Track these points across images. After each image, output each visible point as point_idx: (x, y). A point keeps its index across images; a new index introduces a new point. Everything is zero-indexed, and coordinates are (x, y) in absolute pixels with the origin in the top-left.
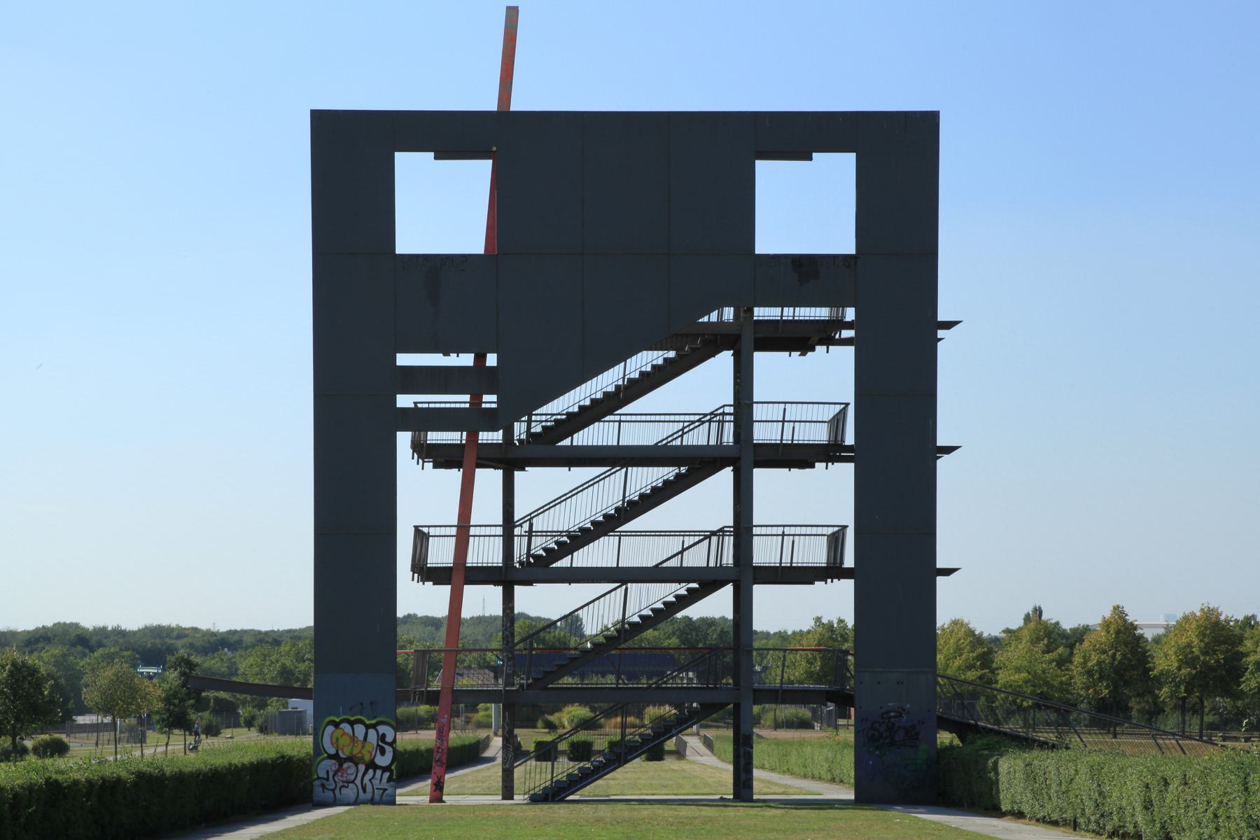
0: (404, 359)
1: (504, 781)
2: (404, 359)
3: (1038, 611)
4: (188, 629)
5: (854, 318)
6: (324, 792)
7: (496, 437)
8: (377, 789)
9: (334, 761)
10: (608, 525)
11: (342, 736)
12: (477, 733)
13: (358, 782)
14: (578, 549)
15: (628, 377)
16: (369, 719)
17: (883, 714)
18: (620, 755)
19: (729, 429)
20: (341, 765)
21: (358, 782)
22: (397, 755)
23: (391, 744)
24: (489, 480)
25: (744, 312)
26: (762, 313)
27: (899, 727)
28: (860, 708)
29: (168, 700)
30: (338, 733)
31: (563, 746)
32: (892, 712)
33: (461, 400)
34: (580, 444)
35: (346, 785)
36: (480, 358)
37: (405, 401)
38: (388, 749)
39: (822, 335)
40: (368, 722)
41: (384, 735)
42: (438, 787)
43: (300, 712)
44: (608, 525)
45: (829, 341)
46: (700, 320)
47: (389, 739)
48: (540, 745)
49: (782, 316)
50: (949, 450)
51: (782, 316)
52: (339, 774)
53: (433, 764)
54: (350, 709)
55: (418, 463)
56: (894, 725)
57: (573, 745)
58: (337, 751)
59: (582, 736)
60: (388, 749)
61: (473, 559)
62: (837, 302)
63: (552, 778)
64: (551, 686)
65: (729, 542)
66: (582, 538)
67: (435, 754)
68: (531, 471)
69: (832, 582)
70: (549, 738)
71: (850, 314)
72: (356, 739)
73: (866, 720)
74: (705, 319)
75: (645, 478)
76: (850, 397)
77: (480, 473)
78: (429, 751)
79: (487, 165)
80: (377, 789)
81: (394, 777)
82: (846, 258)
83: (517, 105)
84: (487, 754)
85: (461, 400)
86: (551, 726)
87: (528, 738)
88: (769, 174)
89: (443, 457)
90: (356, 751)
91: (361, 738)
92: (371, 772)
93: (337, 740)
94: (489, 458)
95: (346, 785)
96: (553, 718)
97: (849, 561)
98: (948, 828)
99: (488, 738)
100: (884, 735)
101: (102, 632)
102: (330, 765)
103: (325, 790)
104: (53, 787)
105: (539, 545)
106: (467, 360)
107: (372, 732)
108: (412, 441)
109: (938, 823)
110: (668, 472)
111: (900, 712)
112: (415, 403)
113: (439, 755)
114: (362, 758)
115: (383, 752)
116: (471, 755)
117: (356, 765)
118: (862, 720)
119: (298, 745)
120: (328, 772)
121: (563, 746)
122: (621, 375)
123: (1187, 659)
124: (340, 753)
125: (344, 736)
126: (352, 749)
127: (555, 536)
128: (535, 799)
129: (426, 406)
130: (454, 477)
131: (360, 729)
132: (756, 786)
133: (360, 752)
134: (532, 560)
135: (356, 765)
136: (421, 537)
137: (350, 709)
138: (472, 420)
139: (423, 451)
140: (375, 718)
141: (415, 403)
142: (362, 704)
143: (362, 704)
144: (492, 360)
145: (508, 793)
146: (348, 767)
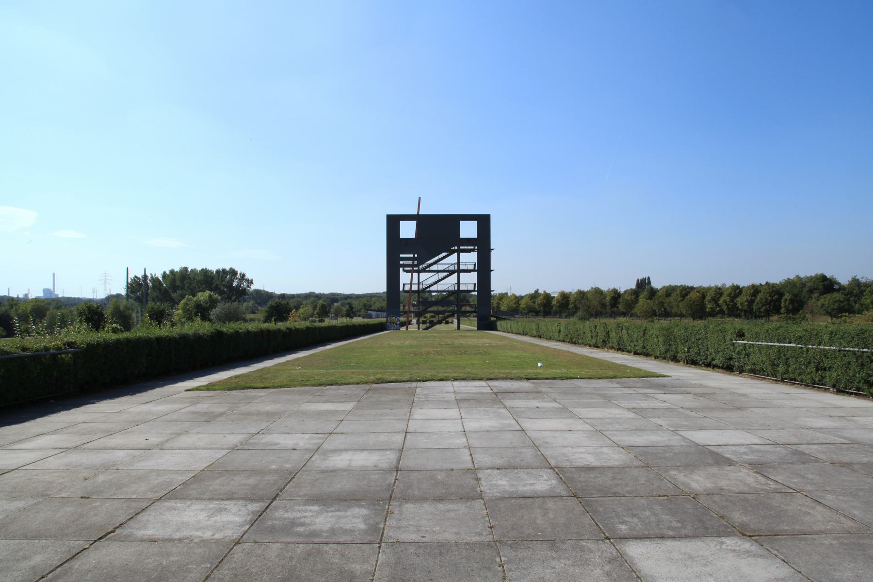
0: (401, 256)
2: (401, 256)
3: (538, 290)
10: (436, 283)
18: (440, 322)
19: (456, 266)
24: (415, 275)
25: (459, 247)
26: (461, 247)
29: (347, 311)
31: (428, 321)
33: (411, 262)
36: (414, 255)
37: (401, 262)
39: (473, 250)
42: (407, 327)
44: (436, 283)
45: (474, 251)
48: (423, 321)
50: (493, 270)
57: (430, 321)
59: (432, 319)
61: (413, 289)
62: (474, 246)
65: (456, 285)
66: (431, 285)
68: (422, 273)
70: (424, 320)
71: (476, 248)
79: (415, 222)
82: (475, 238)
83: (420, 213)
84: (412, 323)
85: (411, 262)
86: (425, 317)
87: (422, 319)
88: (462, 223)
89: (407, 271)
96: (425, 315)
98: (493, 334)
102: (390, 323)
106: (412, 256)
110: (446, 274)
119: (384, 320)
121: (428, 321)
123: (558, 302)
128: (423, 330)
131: (394, 318)
136: (404, 285)
138: (413, 266)
139: (404, 271)
144: (416, 256)
145: (419, 328)
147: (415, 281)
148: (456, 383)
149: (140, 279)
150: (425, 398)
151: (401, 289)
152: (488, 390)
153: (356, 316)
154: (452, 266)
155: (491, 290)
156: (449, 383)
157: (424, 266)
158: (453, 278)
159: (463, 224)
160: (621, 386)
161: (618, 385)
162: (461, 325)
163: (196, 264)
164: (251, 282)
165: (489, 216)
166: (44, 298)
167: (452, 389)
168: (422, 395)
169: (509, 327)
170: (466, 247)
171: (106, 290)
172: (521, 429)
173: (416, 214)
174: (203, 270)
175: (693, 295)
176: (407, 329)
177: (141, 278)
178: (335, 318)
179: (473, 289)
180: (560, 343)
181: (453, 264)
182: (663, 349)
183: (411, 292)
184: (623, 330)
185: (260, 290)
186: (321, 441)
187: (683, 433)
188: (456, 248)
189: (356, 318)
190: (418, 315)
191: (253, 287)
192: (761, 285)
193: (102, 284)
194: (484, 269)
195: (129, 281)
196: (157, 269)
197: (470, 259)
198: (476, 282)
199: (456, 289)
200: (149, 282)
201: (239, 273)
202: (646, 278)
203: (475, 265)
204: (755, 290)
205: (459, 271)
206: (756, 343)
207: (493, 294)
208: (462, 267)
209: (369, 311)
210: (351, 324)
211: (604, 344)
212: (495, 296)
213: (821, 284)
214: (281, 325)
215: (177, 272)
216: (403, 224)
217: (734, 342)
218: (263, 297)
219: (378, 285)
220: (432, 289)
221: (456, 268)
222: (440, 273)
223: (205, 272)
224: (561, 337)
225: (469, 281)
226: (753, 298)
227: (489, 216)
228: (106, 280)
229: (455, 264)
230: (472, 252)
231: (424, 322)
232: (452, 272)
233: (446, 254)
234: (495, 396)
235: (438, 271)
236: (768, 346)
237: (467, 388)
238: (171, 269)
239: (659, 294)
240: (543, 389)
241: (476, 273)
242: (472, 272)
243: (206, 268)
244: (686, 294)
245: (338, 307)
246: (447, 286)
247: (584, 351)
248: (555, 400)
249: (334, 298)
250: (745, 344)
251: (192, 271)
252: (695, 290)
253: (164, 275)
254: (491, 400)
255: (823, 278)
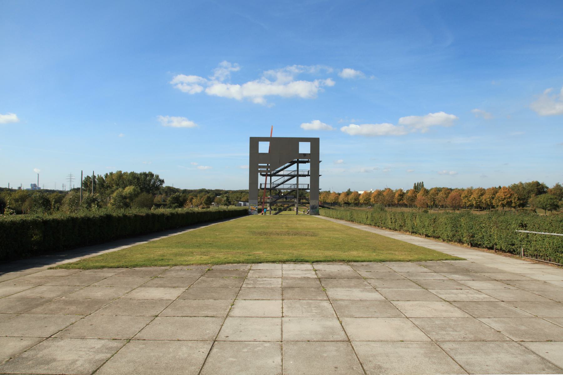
0: (259, 165)
2: (259, 165)
3: (350, 189)
7: (269, 173)
10: (282, 183)
18: (285, 210)
19: (296, 172)
22: (258, 209)
24: (269, 178)
33: (266, 169)
36: (268, 165)
37: (259, 169)
39: (308, 162)
44: (282, 183)
65: (296, 185)
66: (279, 185)
75: (286, 178)
83: (272, 137)
85: (266, 169)
87: (273, 207)
88: (300, 143)
89: (263, 175)
94: (269, 175)
97: (309, 188)
101: (209, 190)
102: (251, 210)
104: (125, 216)
105: (274, 185)
106: (266, 165)
109: (357, 229)
110: (289, 177)
111: (315, 205)
132: (298, 213)
136: (261, 184)
147: (268, 181)
148: (285, 266)
149: (90, 178)
150: (253, 284)
151: (259, 188)
152: (312, 275)
154: (293, 172)
155: (320, 188)
156: (278, 266)
157: (274, 172)
158: (294, 181)
159: (301, 144)
160: (431, 271)
161: (425, 270)
162: (299, 211)
163: (127, 169)
164: (162, 181)
166: (31, 189)
167: (279, 273)
168: (252, 280)
169: (331, 214)
170: (303, 160)
171: (71, 185)
172: (347, 339)
174: (131, 173)
175: (453, 194)
177: (91, 177)
178: (217, 206)
179: (307, 188)
180: (367, 226)
181: (294, 171)
182: (450, 234)
183: (265, 189)
184: (417, 219)
185: (170, 187)
186: (103, 356)
187: (533, 347)
188: (296, 160)
189: (231, 206)
190: (271, 204)
191: (164, 185)
192: (495, 187)
193: (68, 181)
194: (315, 174)
195: (83, 179)
196: (101, 171)
197: (305, 168)
198: (309, 183)
199: (296, 187)
200: (96, 180)
201: (155, 175)
202: (420, 183)
203: (308, 172)
204: (495, 191)
205: (298, 176)
206: (538, 233)
208: (300, 173)
209: (239, 202)
210: (222, 210)
211: (400, 228)
212: (322, 193)
213: (536, 187)
214: (180, 210)
215: (114, 174)
216: (261, 144)
217: (516, 231)
218: (171, 190)
219: (242, 183)
221: (296, 173)
222: (285, 177)
223: (133, 174)
224: (368, 222)
225: (305, 182)
226: (493, 196)
228: (71, 179)
229: (295, 171)
231: (275, 209)
232: (293, 176)
233: (289, 164)
234: (319, 282)
235: (284, 176)
236: (551, 236)
237: (295, 272)
238: (111, 172)
239: (431, 192)
240: (364, 273)
241: (309, 177)
242: (307, 177)
243: (133, 172)
244: (449, 193)
245: (219, 198)
246: (290, 185)
247: (387, 233)
248: (375, 289)
249: (218, 193)
250: (528, 233)
251: (124, 173)
252: (454, 191)
253: (106, 176)
254: (315, 288)
255: (537, 184)
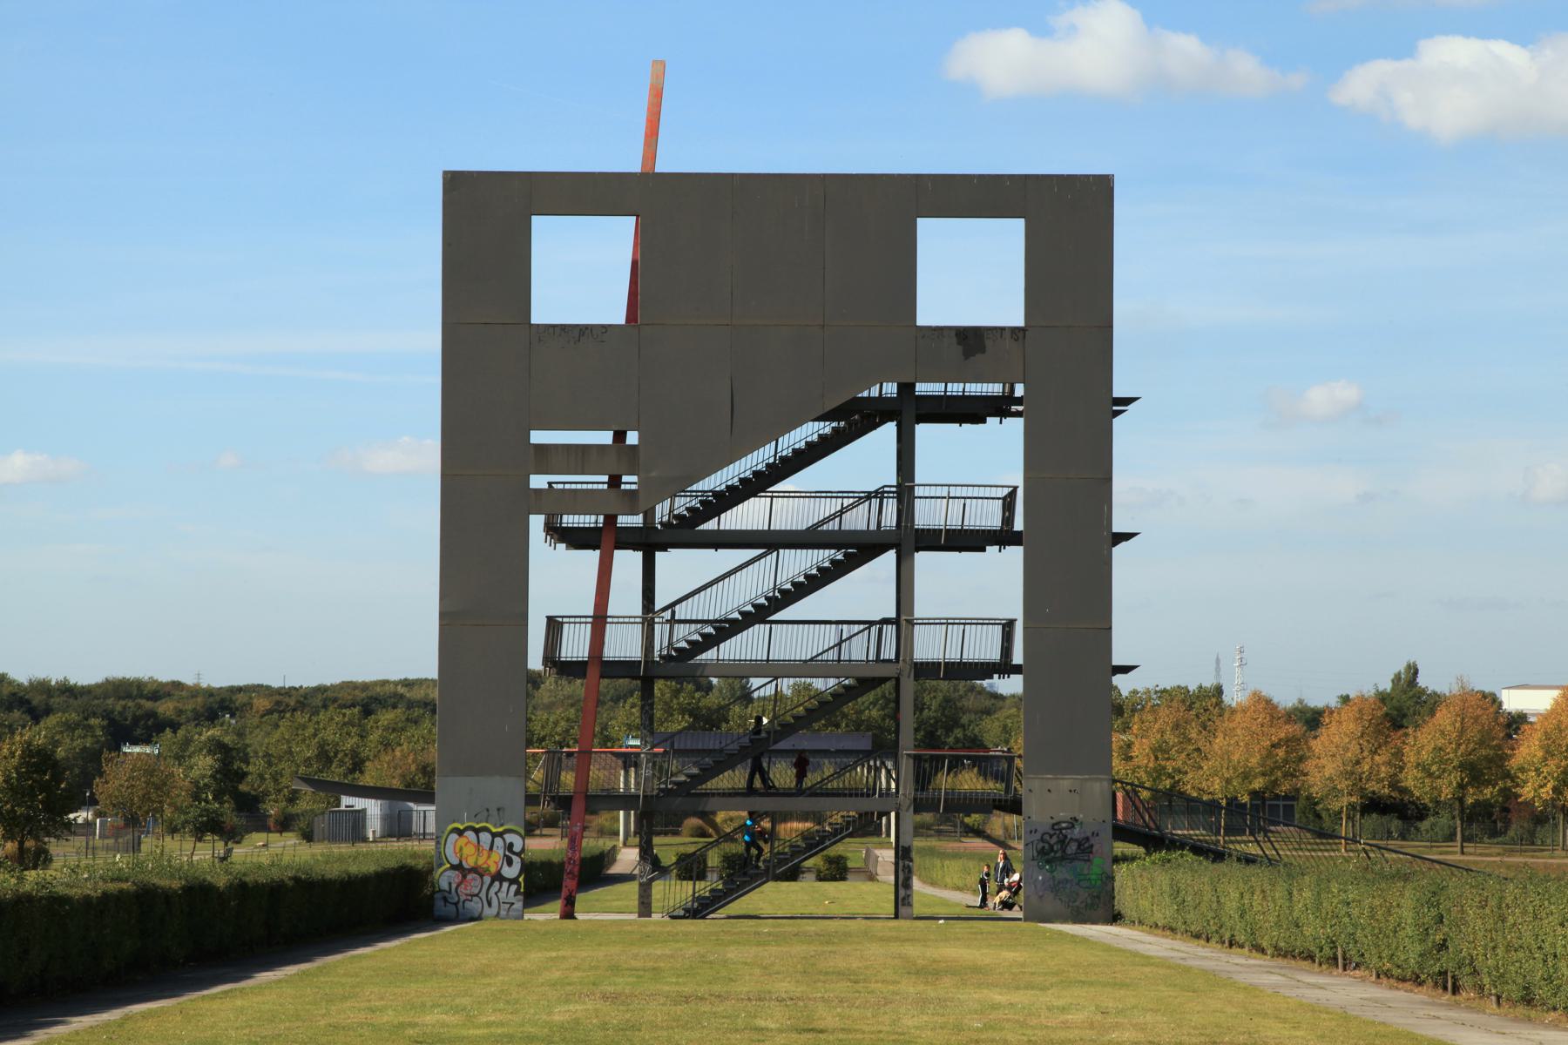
0: (538, 437)
1: (641, 896)
2: (538, 437)
3: (1413, 671)
4: (167, 684)
5: (1023, 394)
6: (445, 906)
7: (636, 520)
8: (504, 903)
9: (457, 872)
10: (760, 614)
11: (466, 845)
12: (240, 852)
13: (483, 895)
14: (724, 641)
15: (780, 454)
16: (495, 826)
17: (1054, 825)
19: (891, 507)
20: (464, 877)
21: (483, 895)
22: (527, 868)
23: (518, 854)
24: (628, 563)
27: (1071, 839)
28: (1029, 818)
30: (462, 841)
32: (1064, 822)
34: (727, 528)
35: (470, 898)
36: (620, 436)
37: (538, 481)
38: (516, 859)
39: (1000, 407)
40: (494, 830)
41: (511, 845)
42: (570, 903)
43: (359, 811)
44: (760, 614)
46: (860, 395)
47: (517, 848)
49: (946, 391)
51: (946, 391)
52: (463, 886)
53: (565, 877)
54: (476, 816)
55: (550, 545)
56: (1066, 837)
58: (461, 861)
60: (516, 859)
63: (694, 893)
64: (693, 791)
65: (890, 631)
66: (727, 629)
67: (566, 865)
68: (674, 553)
69: (1009, 677)
72: (481, 849)
73: (1036, 831)
74: (865, 394)
75: (797, 563)
76: (1017, 479)
77: (619, 555)
78: (562, 865)
80: (504, 903)
81: (522, 890)
82: (1014, 330)
83: (663, 166)
84: (615, 869)
87: (668, 848)
89: (577, 539)
90: (481, 862)
91: (487, 847)
92: (497, 884)
93: (461, 849)
94: (628, 539)
95: (470, 898)
97: (1018, 658)
99: (614, 850)
100: (1055, 848)
102: (455, 876)
103: (448, 904)
106: (606, 438)
107: (498, 841)
108: (545, 524)
110: (822, 557)
111: (1074, 821)
112: (550, 484)
113: (570, 867)
114: (488, 869)
115: (510, 863)
116: (595, 872)
117: (482, 876)
118: (1031, 832)
120: (450, 884)
122: (773, 453)
124: (464, 863)
125: (469, 845)
126: (477, 859)
127: (697, 496)
129: (561, 486)
130: (592, 557)
133: (485, 862)
134: (673, 653)
135: (482, 876)
136: (554, 626)
137: (476, 816)
139: (558, 533)
140: (502, 825)
141: (550, 484)
142: (488, 810)
143: (488, 810)
146: (474, 879)
147: (626, 597)
153: (261, 825)
157: (682, 504)
162: (916, 884)
165: (455, 183)
169: (1231, 905)
170: (955, 388)
173: (636, 167)
176: (568, 914)
179: (993, 654)
181: (869, 496)
188: (890, 389)
189: (258, 838)
199: (889, 652)
203: (1008, 503)
207: (1125, 693)
208: (927, 515)
220: (733, 649)
221: (890, 518)
227: (455, 183)
229: (879, 494)
230: (992, 421)
235: (769, 542)
242: (992, 550)
245: (148, 768)
